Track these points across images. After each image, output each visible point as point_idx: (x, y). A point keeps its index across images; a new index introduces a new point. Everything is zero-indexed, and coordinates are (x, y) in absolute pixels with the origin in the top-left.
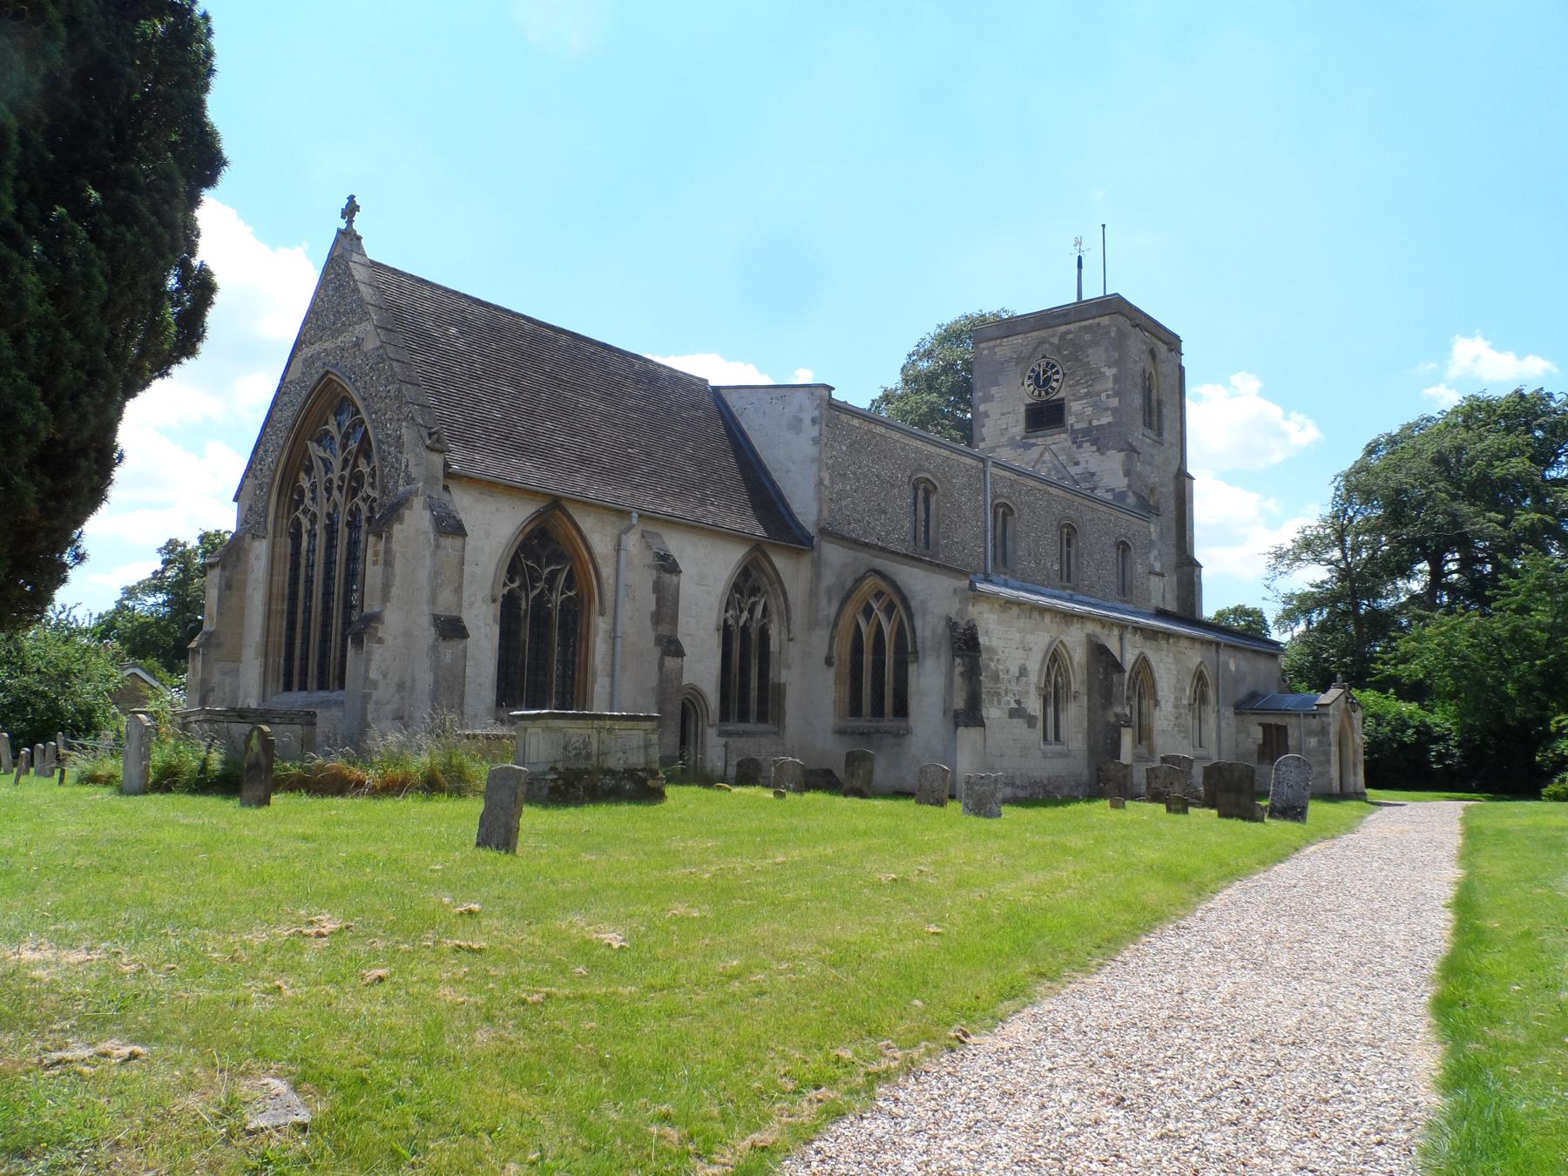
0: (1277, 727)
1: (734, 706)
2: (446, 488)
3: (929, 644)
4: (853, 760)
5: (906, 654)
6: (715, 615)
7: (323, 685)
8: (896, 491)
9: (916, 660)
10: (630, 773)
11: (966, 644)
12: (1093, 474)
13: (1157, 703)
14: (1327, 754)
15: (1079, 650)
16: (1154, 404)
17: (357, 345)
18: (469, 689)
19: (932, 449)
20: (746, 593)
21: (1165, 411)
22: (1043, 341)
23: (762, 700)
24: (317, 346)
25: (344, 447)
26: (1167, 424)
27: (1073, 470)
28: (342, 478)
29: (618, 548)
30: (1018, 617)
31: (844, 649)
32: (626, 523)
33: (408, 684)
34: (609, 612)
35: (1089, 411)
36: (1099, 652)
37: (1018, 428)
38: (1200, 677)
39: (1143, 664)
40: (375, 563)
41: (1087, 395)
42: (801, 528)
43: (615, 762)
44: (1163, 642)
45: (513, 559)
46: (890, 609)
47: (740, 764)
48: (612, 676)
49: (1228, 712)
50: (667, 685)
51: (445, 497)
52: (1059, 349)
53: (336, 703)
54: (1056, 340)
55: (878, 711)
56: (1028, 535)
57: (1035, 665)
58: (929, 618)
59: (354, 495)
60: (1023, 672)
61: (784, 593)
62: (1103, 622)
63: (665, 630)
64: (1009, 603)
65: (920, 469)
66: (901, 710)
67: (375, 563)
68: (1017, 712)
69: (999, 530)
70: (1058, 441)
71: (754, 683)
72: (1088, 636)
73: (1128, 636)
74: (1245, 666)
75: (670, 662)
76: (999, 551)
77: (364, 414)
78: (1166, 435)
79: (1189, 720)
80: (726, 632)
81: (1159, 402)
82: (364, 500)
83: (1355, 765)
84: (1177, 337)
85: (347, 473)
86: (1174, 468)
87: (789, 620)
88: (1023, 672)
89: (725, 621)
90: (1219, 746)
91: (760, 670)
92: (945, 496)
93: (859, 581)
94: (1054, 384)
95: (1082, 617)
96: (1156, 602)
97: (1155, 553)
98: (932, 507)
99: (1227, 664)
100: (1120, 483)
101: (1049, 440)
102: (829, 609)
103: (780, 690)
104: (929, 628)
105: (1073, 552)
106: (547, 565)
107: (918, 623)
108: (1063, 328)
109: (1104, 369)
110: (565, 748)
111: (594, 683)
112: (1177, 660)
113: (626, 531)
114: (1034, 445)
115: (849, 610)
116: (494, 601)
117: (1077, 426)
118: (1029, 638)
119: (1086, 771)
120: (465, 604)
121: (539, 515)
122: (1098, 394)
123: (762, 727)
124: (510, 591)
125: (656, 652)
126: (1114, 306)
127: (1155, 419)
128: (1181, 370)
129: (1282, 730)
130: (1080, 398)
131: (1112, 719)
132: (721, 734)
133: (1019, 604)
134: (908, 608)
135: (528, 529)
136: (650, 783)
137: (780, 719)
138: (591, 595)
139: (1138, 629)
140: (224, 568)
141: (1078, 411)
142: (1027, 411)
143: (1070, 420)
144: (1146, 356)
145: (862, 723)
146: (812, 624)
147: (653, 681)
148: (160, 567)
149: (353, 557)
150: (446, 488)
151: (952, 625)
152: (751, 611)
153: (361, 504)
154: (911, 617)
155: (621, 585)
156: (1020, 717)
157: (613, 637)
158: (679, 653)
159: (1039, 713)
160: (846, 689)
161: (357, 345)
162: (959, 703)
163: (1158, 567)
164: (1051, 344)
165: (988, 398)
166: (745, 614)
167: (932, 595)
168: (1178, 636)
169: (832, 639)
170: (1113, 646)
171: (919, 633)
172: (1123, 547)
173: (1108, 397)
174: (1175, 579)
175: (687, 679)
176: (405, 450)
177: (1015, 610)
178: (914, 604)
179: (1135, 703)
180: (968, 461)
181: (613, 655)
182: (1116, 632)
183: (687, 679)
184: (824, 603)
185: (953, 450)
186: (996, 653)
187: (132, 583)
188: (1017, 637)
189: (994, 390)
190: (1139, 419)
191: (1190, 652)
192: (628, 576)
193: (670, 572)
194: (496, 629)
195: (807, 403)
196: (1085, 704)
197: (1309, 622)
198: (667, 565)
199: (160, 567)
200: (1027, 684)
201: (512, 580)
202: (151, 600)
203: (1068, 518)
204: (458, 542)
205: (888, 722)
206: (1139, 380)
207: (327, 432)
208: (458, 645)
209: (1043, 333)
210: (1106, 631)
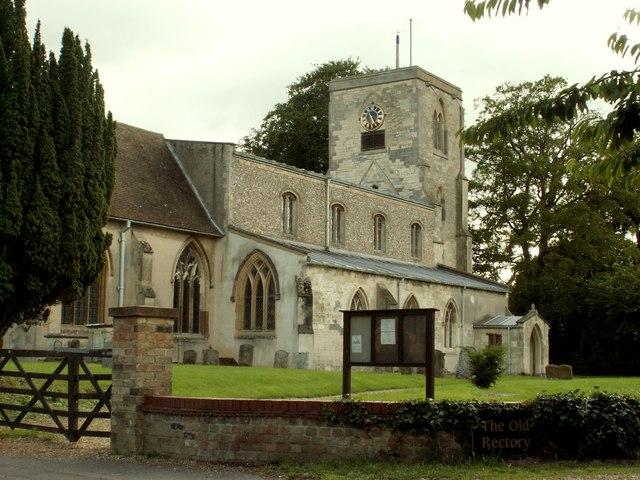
3: (286, 290)
4: (242, 350)
5: (274, 294)
11: (306, 294)
12: (401, 179)
14: (522, 350)
20: (187, 261)
23: (196, 320)
31: (241, 292)
37: (356, 144)
46: (266, 270)
52: (382, 99)
54: (380, 93)
55: (259, 323)
66: (272, 326)
70: (380, 157)
78: (450, 153)
83: (542, 358)
91: (195, 304)
93: (249, 256)
96: (438, 260)
99: (468, 300)
100: (418, 186)
101: (376, 157)
103: (206, 314)
104: (285, 281)
105: (382, 230)
107: (281, 280)
108: (384, 86)
123: (195, 336)
126: (414, 73)
129: (499, 337)
134: (275, 271)
137: (206, 331)
142: (362, 137)
151: (297, 281)
152: (190, 272)
154: (277, 276)
162: (301, 321)
166: (186, 273)
167: (287, 265)
171: (281, 284)
174: (455, 245)
177: (334, 272)
178: (278, 269)
180: (316, 181)
189: (342, 122)
205: (265, 333)
206: (431, 120)
209: (373, 88)
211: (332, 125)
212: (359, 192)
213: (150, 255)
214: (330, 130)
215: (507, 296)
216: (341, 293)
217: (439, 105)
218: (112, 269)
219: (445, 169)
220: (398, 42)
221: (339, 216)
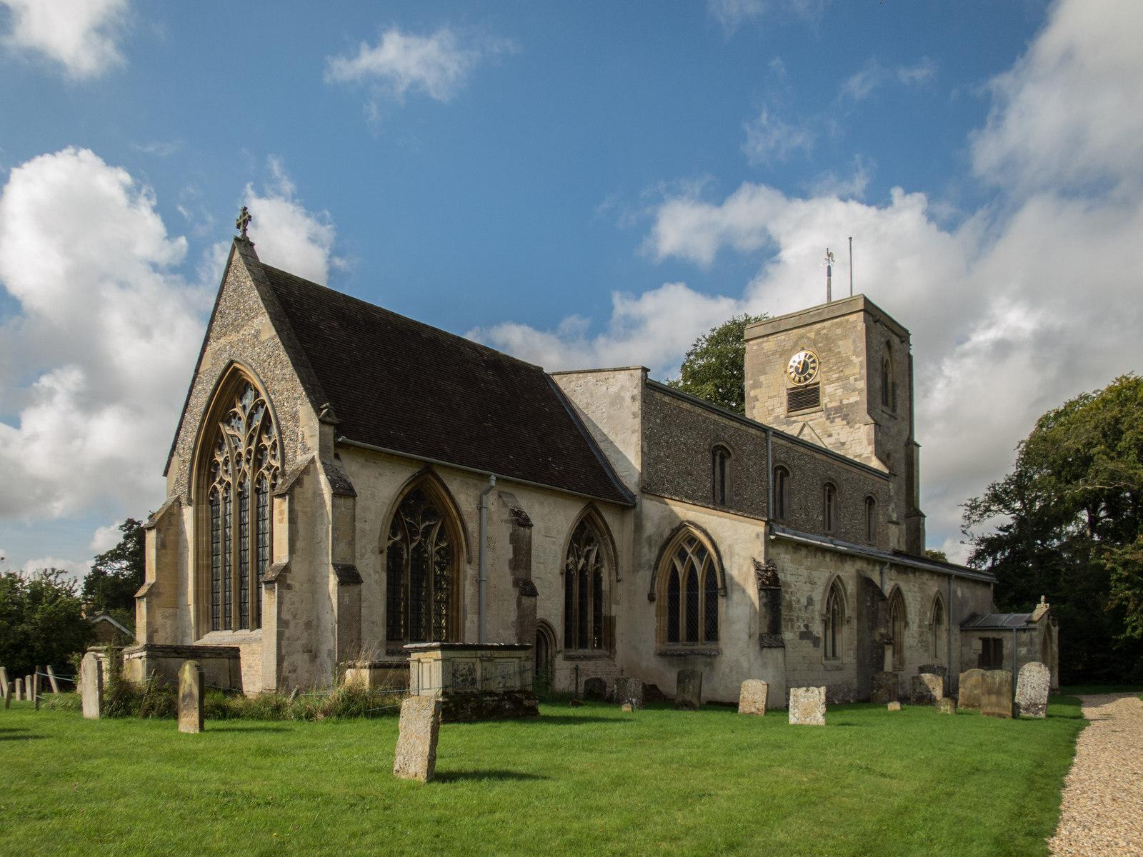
0: (995, 640)
1: (576, 635)
2: (337, 456)
6: (559, 562)
7: (242, 626)
8: (699, 456)
9: (725, 595)
10: (509, 694)
12: (843, 444)
13: (907, 624)
16: (890, 386)
17: (256, 336)
18: (364, 626)
19: (726, 422)
21: (898, 392)
22: (802, 337)
24: (222, 340)
25: (249, 425)
28: (249, 452)
29: (480, 508)
30: (806, 557)
31: (662, 587)
32: (485, 486)
33: (314, 623)
34: (475, 560)
35: (840, 392)
36: (866, 584)
38: (937, 603)
39: (897, 592)
40: (281, 521)
41: (838, 379)
42: (626, 489)
43: (497, 686)
44: (911, 575)
45: (395, 516)
47: (587, 683)
48: (479, 613)
49: (956, 630)
50: (526, 618)
51: (337, 463)
53: (256, 640)
54: (812, 335)
56: (799, 491)
57: (819, 595)
58: (736, 559)
59: (260, 466)
60: (810, 601)
61: (613, 543)
63: (521, 573)
64: (798, 546)
65: (718, 438)
66: (712, 634)
67: (281, 521)
68: (806, 635)
69: (778, 489)
71: (590, 617)
72: (858, 571)
73: (886, 571)
74: (968, 593)
75: (526, 601)
76: (778, 506)
77: (264, 396)
78: (899, 411)
79: (930, 638)
80: (568, 575)
81: (894, 385)
82: (268, 469)
84: (907, 332)
85: (253, 447)
86: (905, 438)
87: (617, 564)
88: (810, 601)
89: (567, 566)
90: (950, 656)
97: (892, 506)
99: (955, 592)
102: (649, 555)
103: (611, 622)
106: (423, 521)
109: (853, 358)
110: (454, 675)
111: (465, 618)
112: (921, 590)
113: (486, 492)
114: (795, 422)
115: (667, 554)
116: (381, 552)
117: (829, 405)
118: (815, 574)
119: (855, 680)
120: (358, 555)
121: (414, 479)
122: (847, 378)
123: (597, 652)
124: (395, 544)
125: (513, 593)
127: (890, 398)
128: (910, 357)
129: (998, 643)
130: (833, 382)
131: (877, 638)
132: (567, 658)
133: (807, 546)
135: (406, 491)
136: (526, 703)
137: (611, 645)
138: (459, 545)
140: (159, 531)
141: (830, 394)
142: (789, 395)
143: (824, 400)
144: (883, 346)
145: (678, 647)
146: (637, 567)
147: (513, 616)
148: (122, 541)
149: (259, 517)
150: (337, 456)
152: (587, 558)
153: (266, 473)
155: (484, 539)
156: (808, 638)
157: (479, 581)
158: (533, 593)
159: (821, 635)
160: (665, 620)
161: (256, 336)
163: (894, 517)
164: (808, 338)
165: (757, 385)
166: (582, 560)
168: (922, 571)
169: (653, 579)
170: (876, 578)
172: (870, 501)
173: (856, 380)
175: (540, 614)
176: (301, 424)
177: (804, 552)
179: (890, 625)
181: (480, 596)
182: (878, 568)
183: (540, 614)
184: (645, 550)
186: (789, 586)
187: (103, 553)
188: (806, 573)
189: (762, 378)
191: (931, 583)
192: (489, 530)
193: (524, 526)
194: (384, 576)
195: (628, 384)
196: (855, 627)
197: (994, 560)
198: (521, 521)
199: (122, 541)
200: (813, 611)
201: (395, 535)
202: (117, 566)
203: (830, 478)
204: (349, 502)
205: (701, 646)
207: (235, 414)
208: (355, 589)
210: (870, 567)
211: (748, 383)
212: (806, 451)
213: (527, 530)
214: (747, 389)
215: (992, 587)
216: (813, 583)
217: (886, 349)
218: (468, 553)
219: (894, 431)
220: (829, 275)
221: (782, 481)
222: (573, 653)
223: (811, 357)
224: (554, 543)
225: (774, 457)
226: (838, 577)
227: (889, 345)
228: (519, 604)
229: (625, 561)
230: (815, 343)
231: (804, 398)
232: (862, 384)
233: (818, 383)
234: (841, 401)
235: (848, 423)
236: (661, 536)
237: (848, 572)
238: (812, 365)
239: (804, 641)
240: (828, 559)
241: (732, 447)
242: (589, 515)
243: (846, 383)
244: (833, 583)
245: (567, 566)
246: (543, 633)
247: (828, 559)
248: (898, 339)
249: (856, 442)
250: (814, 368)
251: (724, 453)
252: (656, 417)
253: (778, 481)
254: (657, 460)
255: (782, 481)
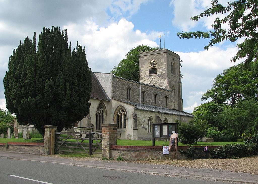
1: (98, 127)
15: (154, 117)
16: (174, 69)
21: (176, 70)
26: (176, 72)
27: (158, 82)
37: (148, 73)
46: (123, 111)
58: (129, 113)
60: (144, 121)
62: (159, 113)
64: (142, 110)
66: (125, 127)
68: (143, 127)
70: (155, 77)
76: (143, 99)
78: (176, 75)
88: (144, 121)
92: (132, 90)
94: (155, 65)
95: (155, 112)
96: (173, 107)
98: (130, 93)
112: (172, 118)
117: (159, 74)
127: (174, 71)
133: (144, 110)
139: (165, 113)
141: (159, 71)
143: (158, 72)
147: (87, 123)
158: (91, 119)
163: (173, 101)
172: (166, 97)
175: (92, 123)
177: (143, 111)
178: (127, 111)
183: (92, 123)
185: (134, 82)
186: (140, 118)
188: (143, 115)
189: (143, 66)
190: (171, 72)
206: (171, 65)
219: (175, 80)
220: (160, 41)
221: (144, 94)
222: (97, 130)
223: (155, 62)
224: (94, 109)
225: (141, 89)
226: (151, 116)
227: (173, 59)
228: (88, 121)
229: (108, 112)
230: (156, 59)
231: (153, 71)
232: (166, 69)
233: (156, 68)
234: (161, 73)
235: (163, 78)
236: (115, 107)
237: (153, 115)
238: (155, 64)
239: (143, 129)
240: (149, 112)
241: (131, 88)
242: (101, 103)
243: (162, 69)
244: (150, 117)
245: (97, 113)
246: (92, 126)
247: (149, 112)
248: (176, 58)
249: (164, 83)
250: (155, 65)
251: (130, 89)
252: (115, 83)
253: (143, 94)
254: (115, 92)
255: (144, 94)
